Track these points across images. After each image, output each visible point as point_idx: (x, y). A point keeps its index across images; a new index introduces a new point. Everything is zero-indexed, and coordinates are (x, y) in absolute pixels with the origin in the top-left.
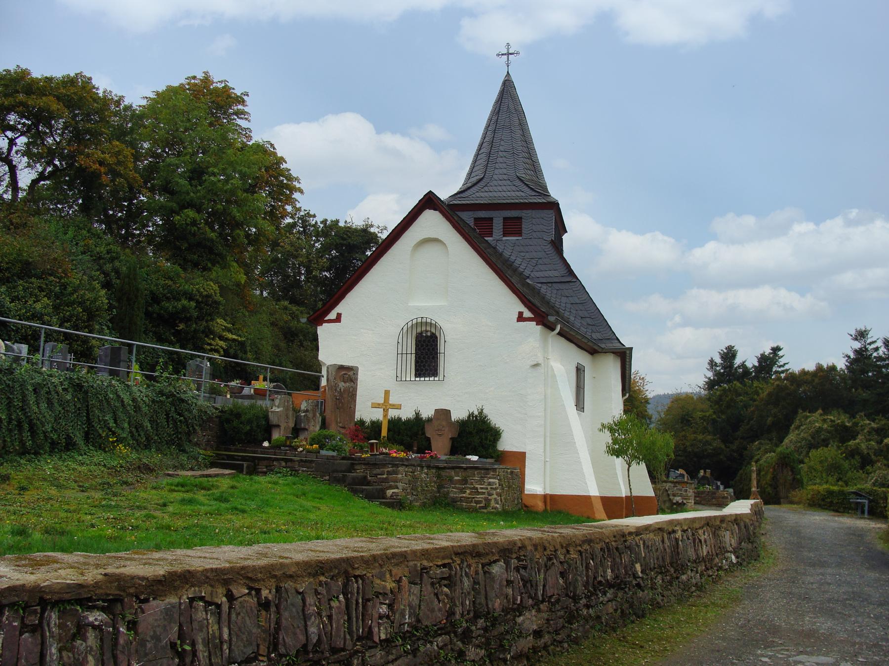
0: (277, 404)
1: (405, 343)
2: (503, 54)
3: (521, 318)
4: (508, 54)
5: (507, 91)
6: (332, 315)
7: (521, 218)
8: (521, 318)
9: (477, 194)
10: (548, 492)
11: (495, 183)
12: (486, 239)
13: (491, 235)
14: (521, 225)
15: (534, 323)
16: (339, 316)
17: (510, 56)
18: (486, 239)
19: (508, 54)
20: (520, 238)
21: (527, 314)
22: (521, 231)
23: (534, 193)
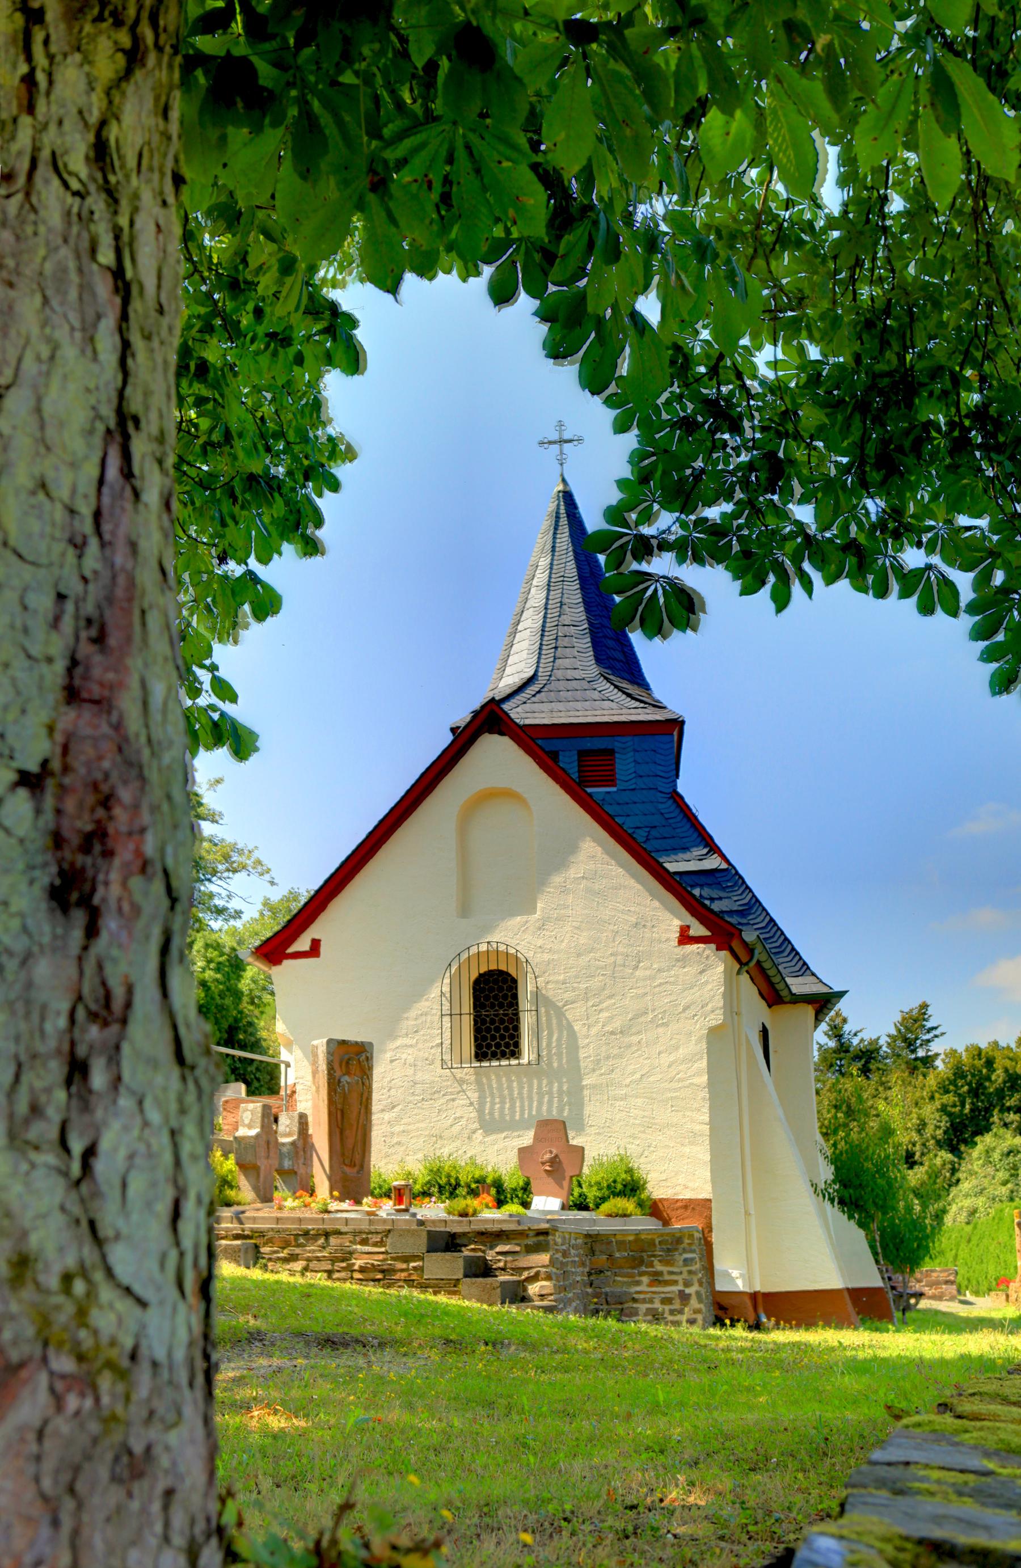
0: (247, 1122)
1: (456, 997)
2: (550, 443)
3: (685, 938)
4: (562, 441)
5: (810, 597)
6: (303, 944)
7: (611, 752)
8: (685, 938)
9: (527, 707)
10: (758, 1288)
11: (561, 685)
12: (589, 790)
13: (610, 780)
14: (613, 765)
15: (713, 946)
16: (316, 944)
17: (555, 437)
18: (589, 790)
19: (562, 441)
20: (614, 789)
21: (698, 929)
22: (614, 775)
23: (637, 704)
